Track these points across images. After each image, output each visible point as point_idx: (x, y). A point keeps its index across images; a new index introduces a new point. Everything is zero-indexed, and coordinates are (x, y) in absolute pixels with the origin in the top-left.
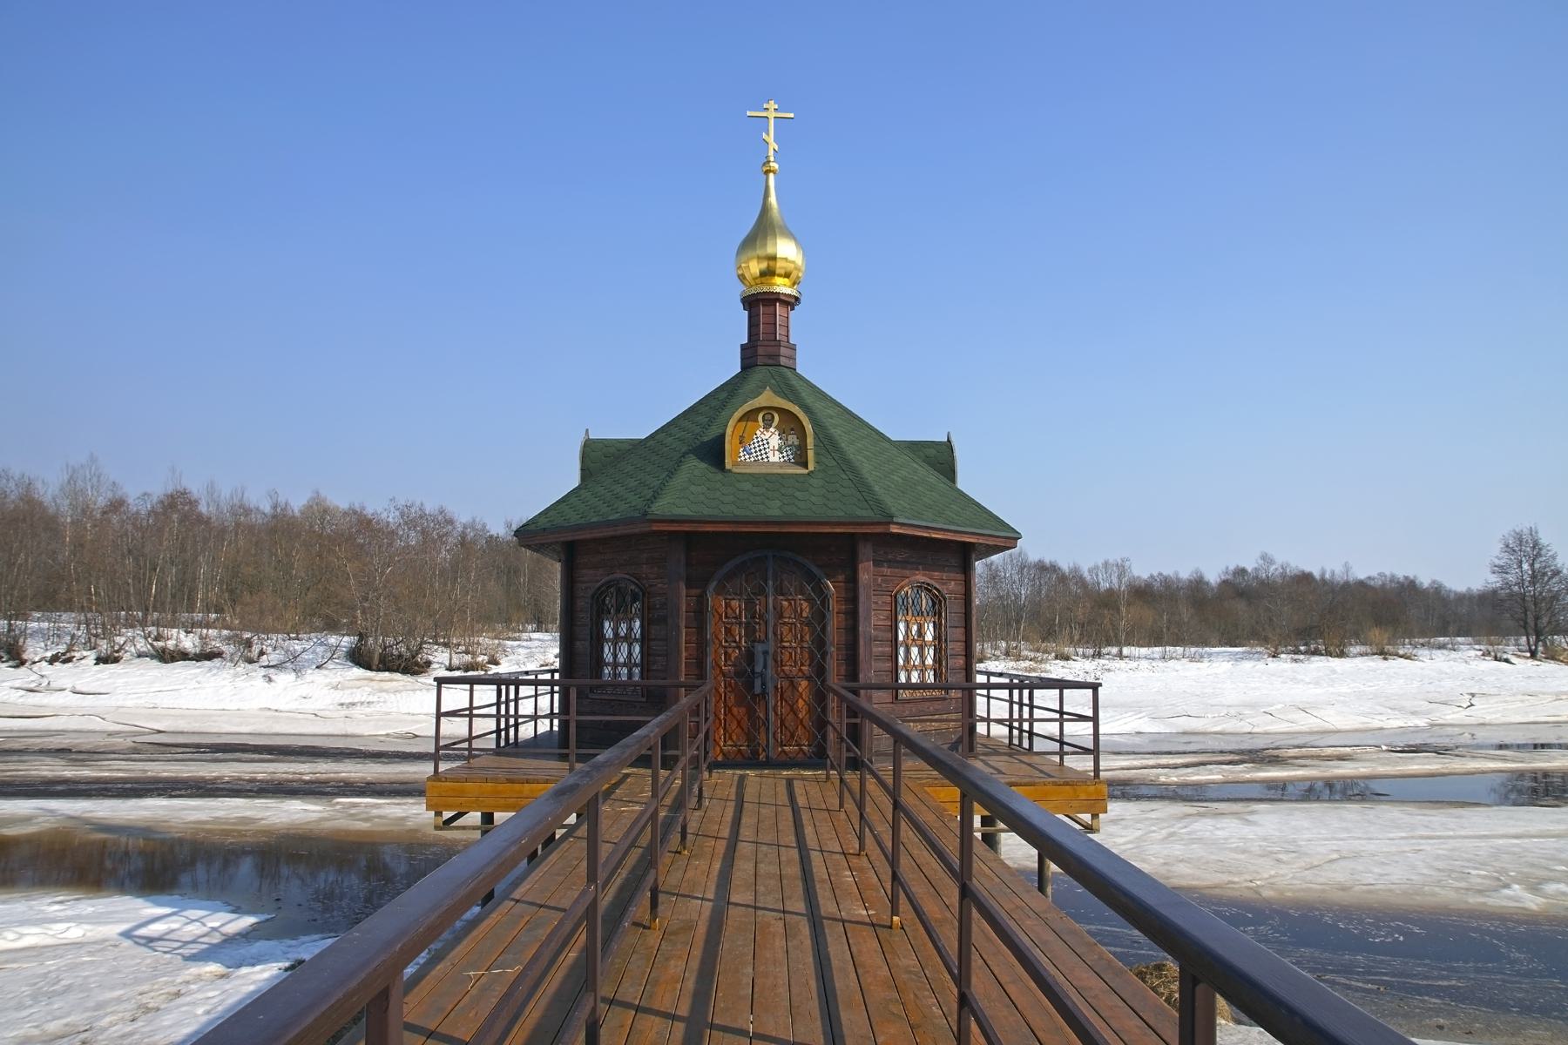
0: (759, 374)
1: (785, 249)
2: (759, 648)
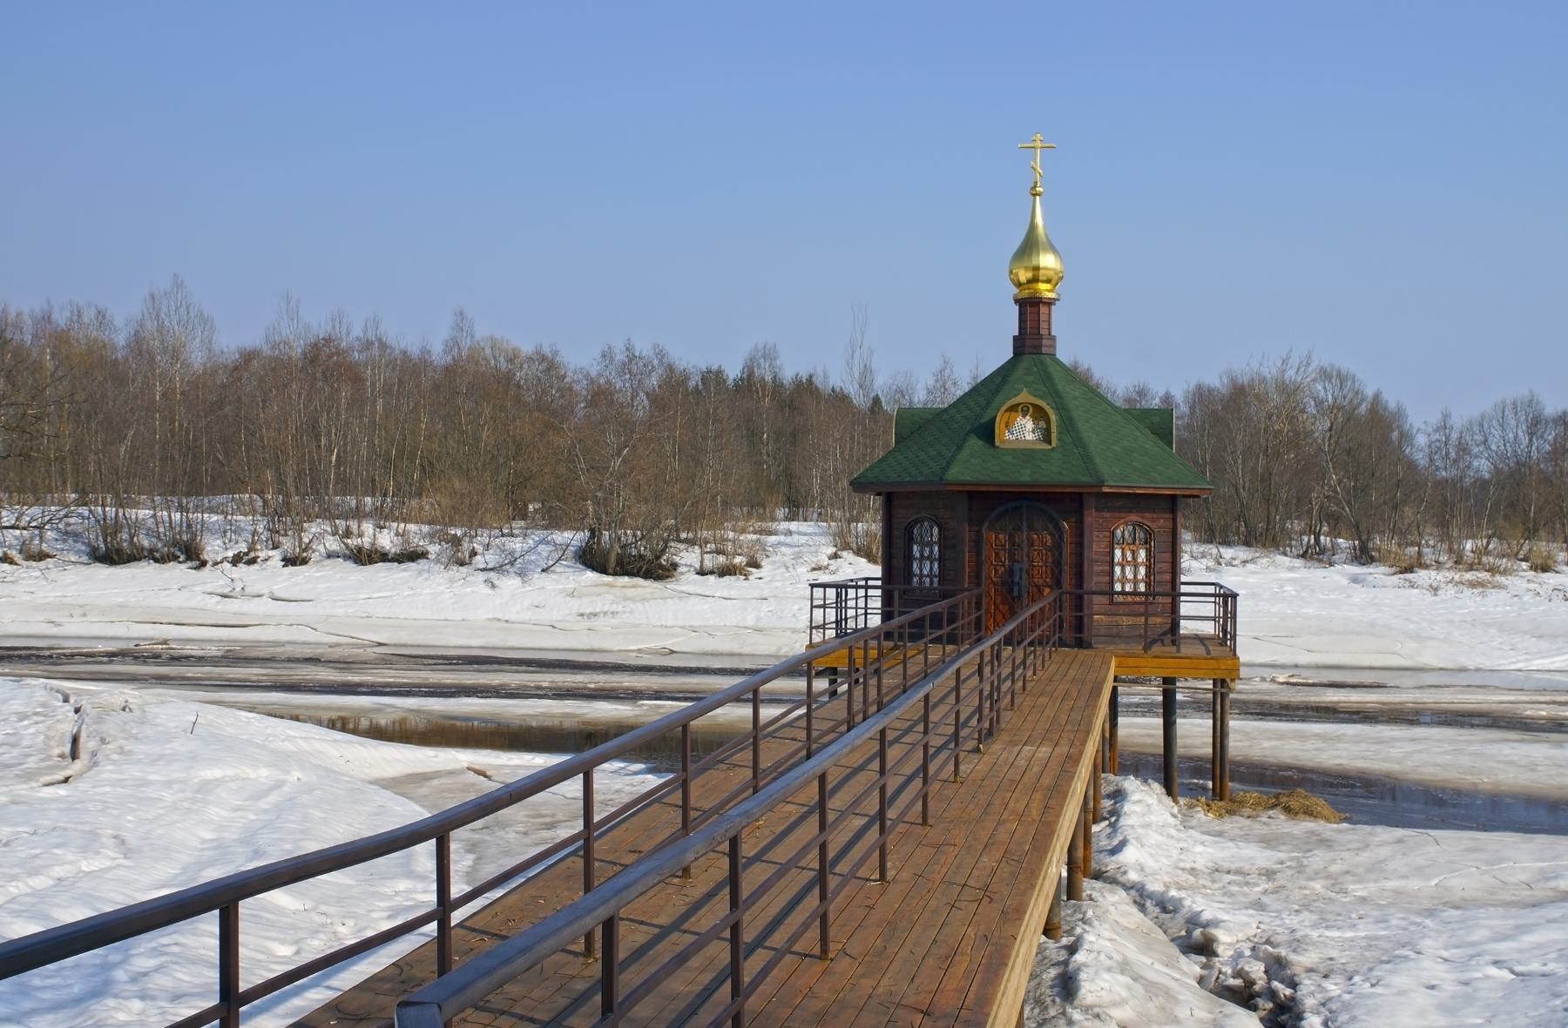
0: (1026, 361)
1: (1047, 261)
2: (1017, 566)
